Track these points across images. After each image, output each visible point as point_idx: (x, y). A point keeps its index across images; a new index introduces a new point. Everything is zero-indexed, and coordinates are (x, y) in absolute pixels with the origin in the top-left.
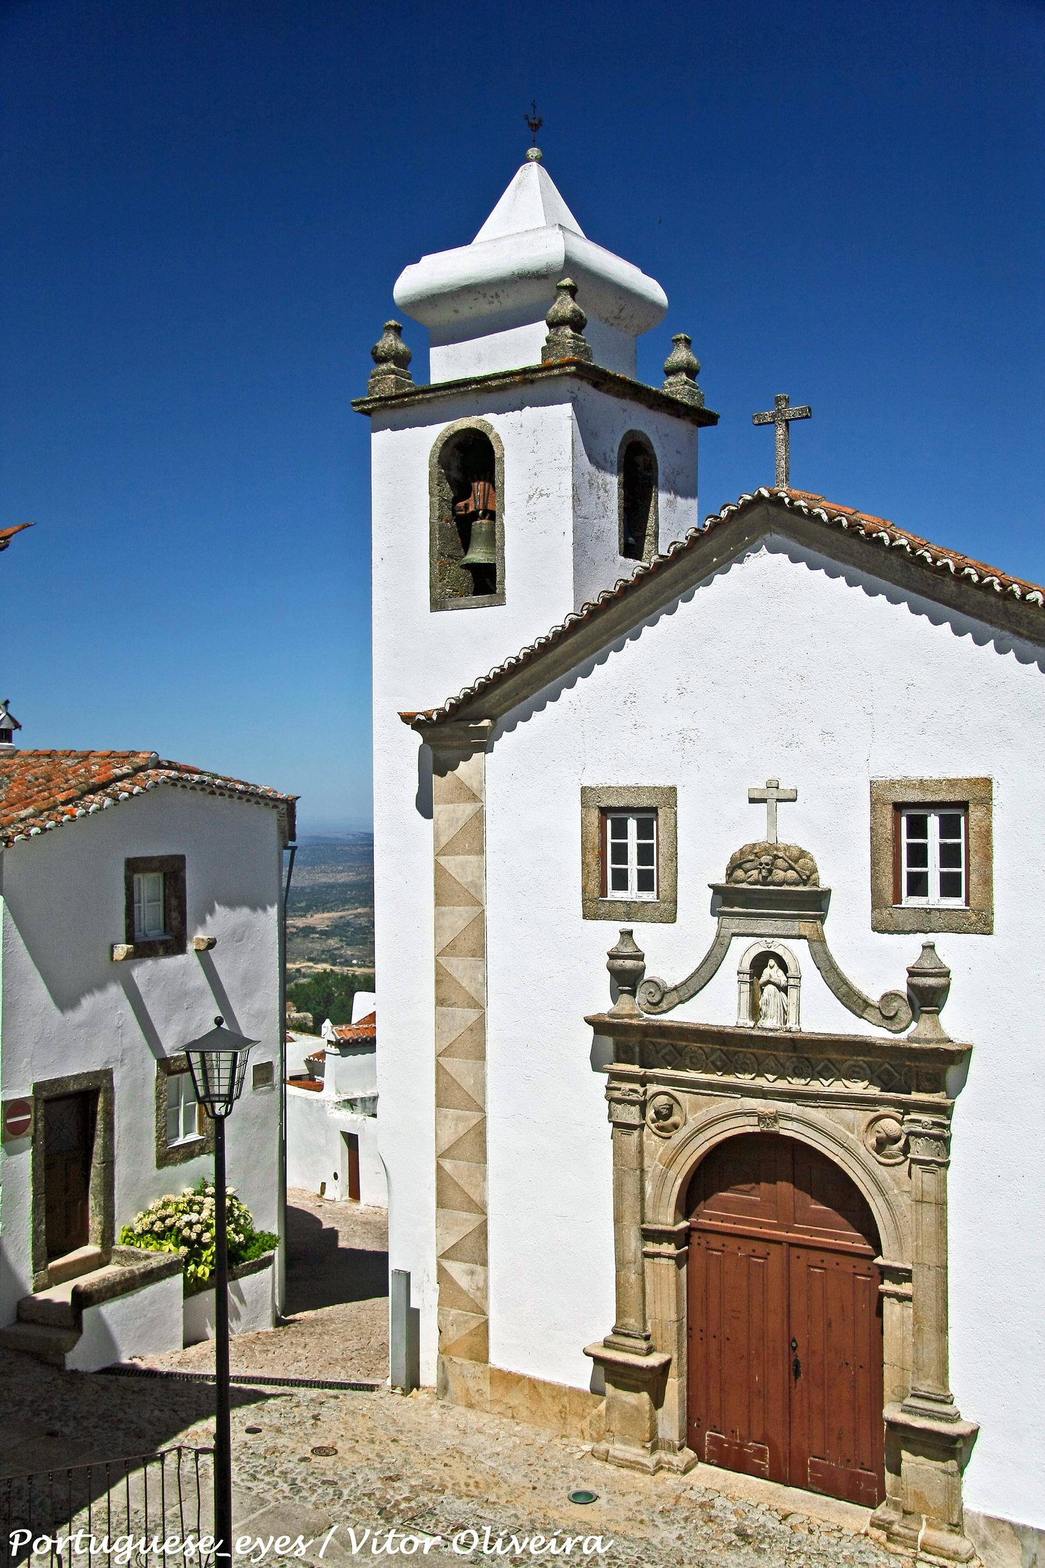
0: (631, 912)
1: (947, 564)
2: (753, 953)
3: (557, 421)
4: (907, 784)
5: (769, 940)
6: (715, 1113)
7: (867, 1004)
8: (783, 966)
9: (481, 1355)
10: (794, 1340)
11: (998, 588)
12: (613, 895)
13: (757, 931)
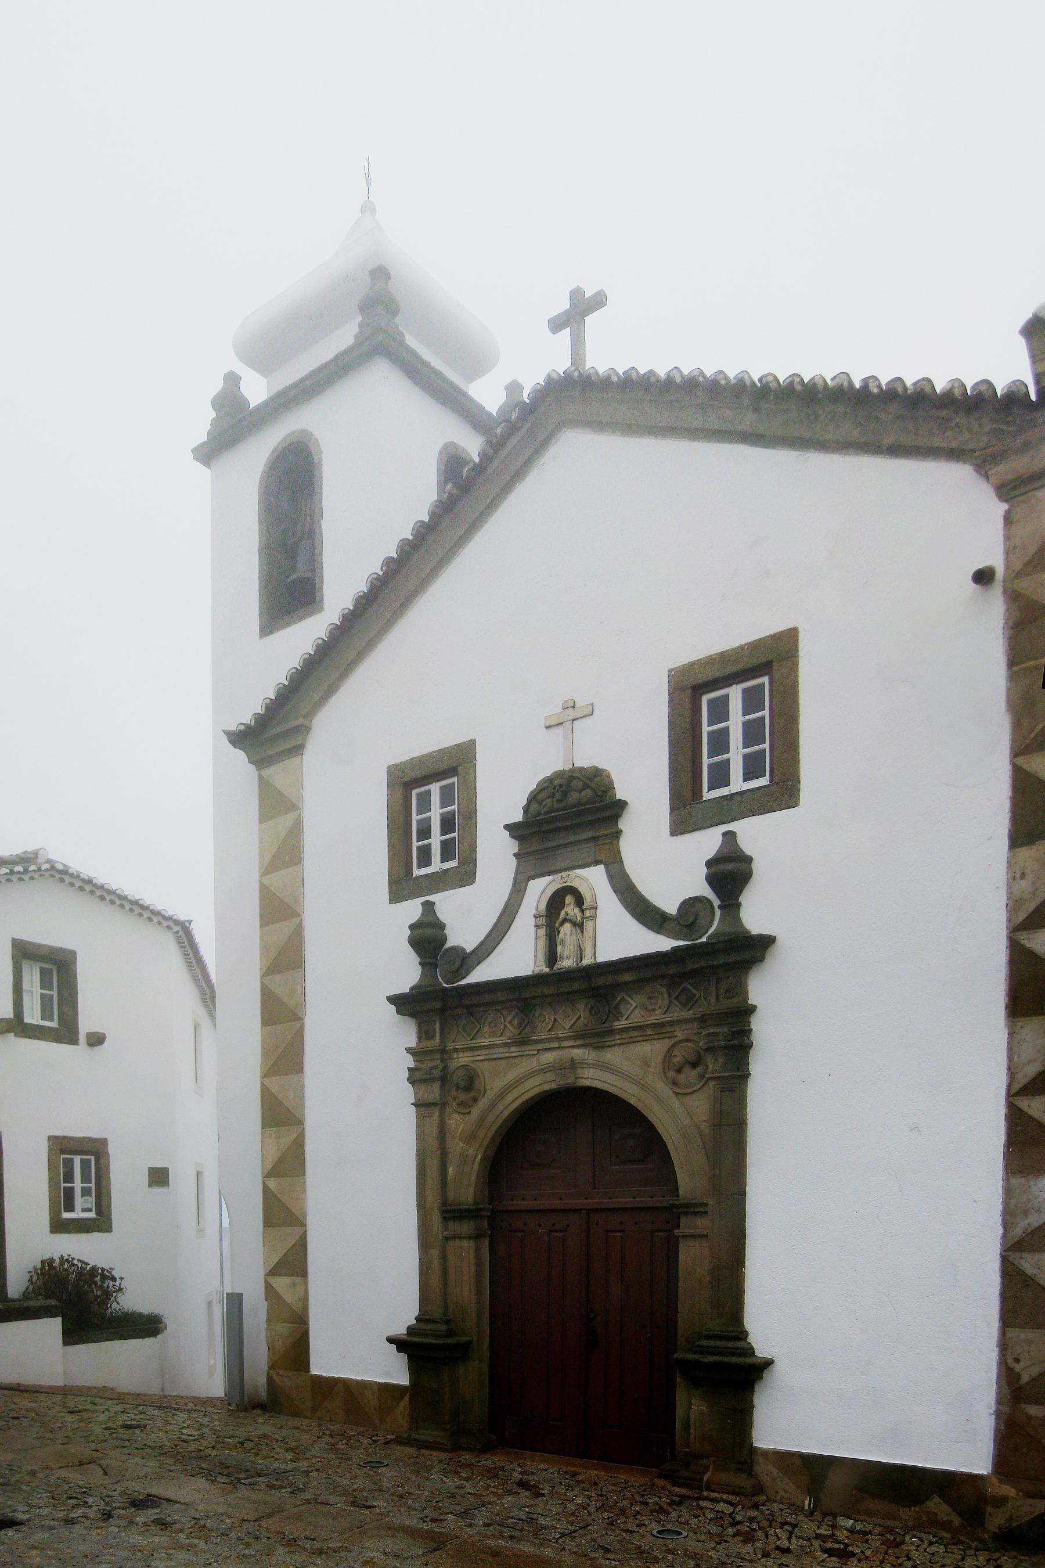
2: (549, 892)
5: (564, 874)
6: (513, 1073)
8: (579, 901)
10: (592, 1311)
13: (552, 868)
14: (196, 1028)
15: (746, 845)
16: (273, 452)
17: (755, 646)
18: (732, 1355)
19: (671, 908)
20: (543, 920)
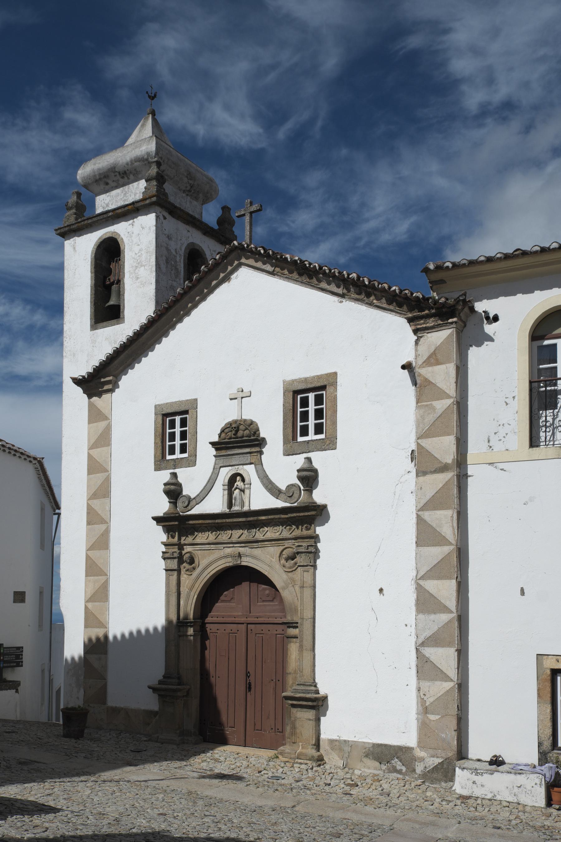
0: (176, 464)
1: (315, 266)
2: (229, 475)
3: (147, 223)
4: (300, 381)
5: (236, 467)
6: (212, 556)
7: (280, 491)
8: (243, 480)
9: (103, 700)
10: (249, 673)
11: (337, 274)
12: (169, 457)
13: (231, 464)
14: (42, 509)
15: (316, 464)
16: (99, 240)
17: (319, 377)
18: (309, 693)
19: (283, 487)
20: (226, 487)
